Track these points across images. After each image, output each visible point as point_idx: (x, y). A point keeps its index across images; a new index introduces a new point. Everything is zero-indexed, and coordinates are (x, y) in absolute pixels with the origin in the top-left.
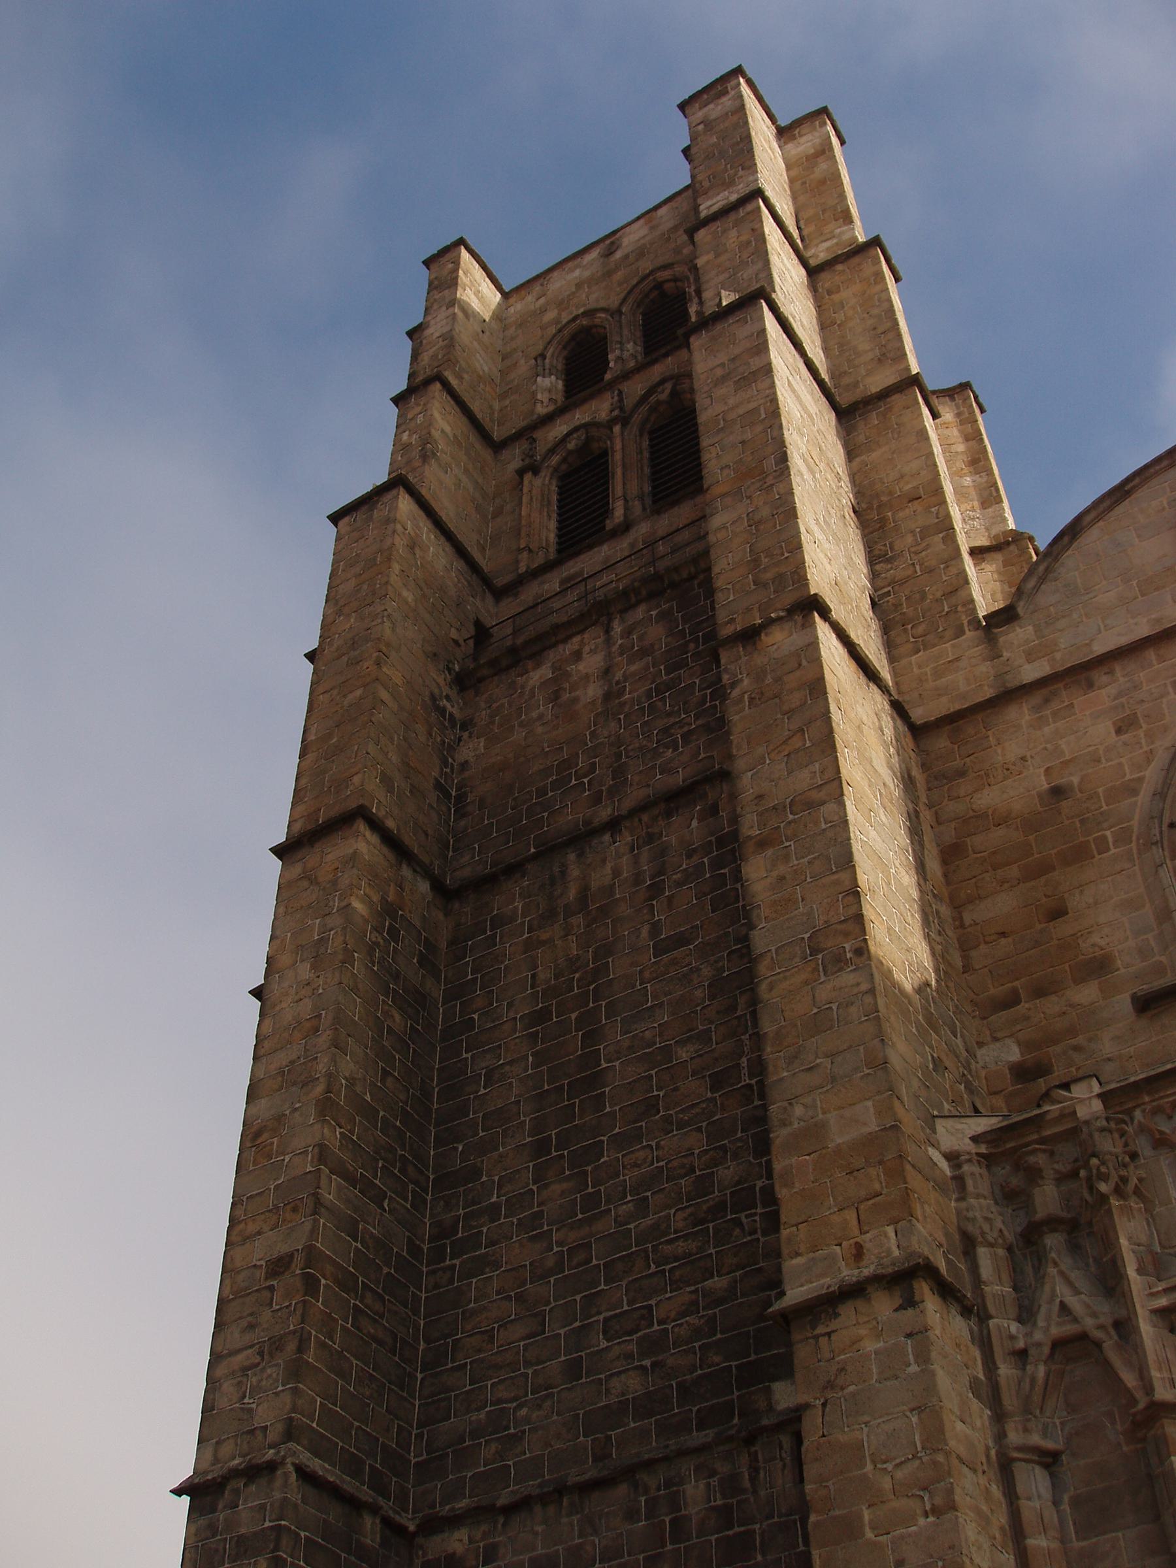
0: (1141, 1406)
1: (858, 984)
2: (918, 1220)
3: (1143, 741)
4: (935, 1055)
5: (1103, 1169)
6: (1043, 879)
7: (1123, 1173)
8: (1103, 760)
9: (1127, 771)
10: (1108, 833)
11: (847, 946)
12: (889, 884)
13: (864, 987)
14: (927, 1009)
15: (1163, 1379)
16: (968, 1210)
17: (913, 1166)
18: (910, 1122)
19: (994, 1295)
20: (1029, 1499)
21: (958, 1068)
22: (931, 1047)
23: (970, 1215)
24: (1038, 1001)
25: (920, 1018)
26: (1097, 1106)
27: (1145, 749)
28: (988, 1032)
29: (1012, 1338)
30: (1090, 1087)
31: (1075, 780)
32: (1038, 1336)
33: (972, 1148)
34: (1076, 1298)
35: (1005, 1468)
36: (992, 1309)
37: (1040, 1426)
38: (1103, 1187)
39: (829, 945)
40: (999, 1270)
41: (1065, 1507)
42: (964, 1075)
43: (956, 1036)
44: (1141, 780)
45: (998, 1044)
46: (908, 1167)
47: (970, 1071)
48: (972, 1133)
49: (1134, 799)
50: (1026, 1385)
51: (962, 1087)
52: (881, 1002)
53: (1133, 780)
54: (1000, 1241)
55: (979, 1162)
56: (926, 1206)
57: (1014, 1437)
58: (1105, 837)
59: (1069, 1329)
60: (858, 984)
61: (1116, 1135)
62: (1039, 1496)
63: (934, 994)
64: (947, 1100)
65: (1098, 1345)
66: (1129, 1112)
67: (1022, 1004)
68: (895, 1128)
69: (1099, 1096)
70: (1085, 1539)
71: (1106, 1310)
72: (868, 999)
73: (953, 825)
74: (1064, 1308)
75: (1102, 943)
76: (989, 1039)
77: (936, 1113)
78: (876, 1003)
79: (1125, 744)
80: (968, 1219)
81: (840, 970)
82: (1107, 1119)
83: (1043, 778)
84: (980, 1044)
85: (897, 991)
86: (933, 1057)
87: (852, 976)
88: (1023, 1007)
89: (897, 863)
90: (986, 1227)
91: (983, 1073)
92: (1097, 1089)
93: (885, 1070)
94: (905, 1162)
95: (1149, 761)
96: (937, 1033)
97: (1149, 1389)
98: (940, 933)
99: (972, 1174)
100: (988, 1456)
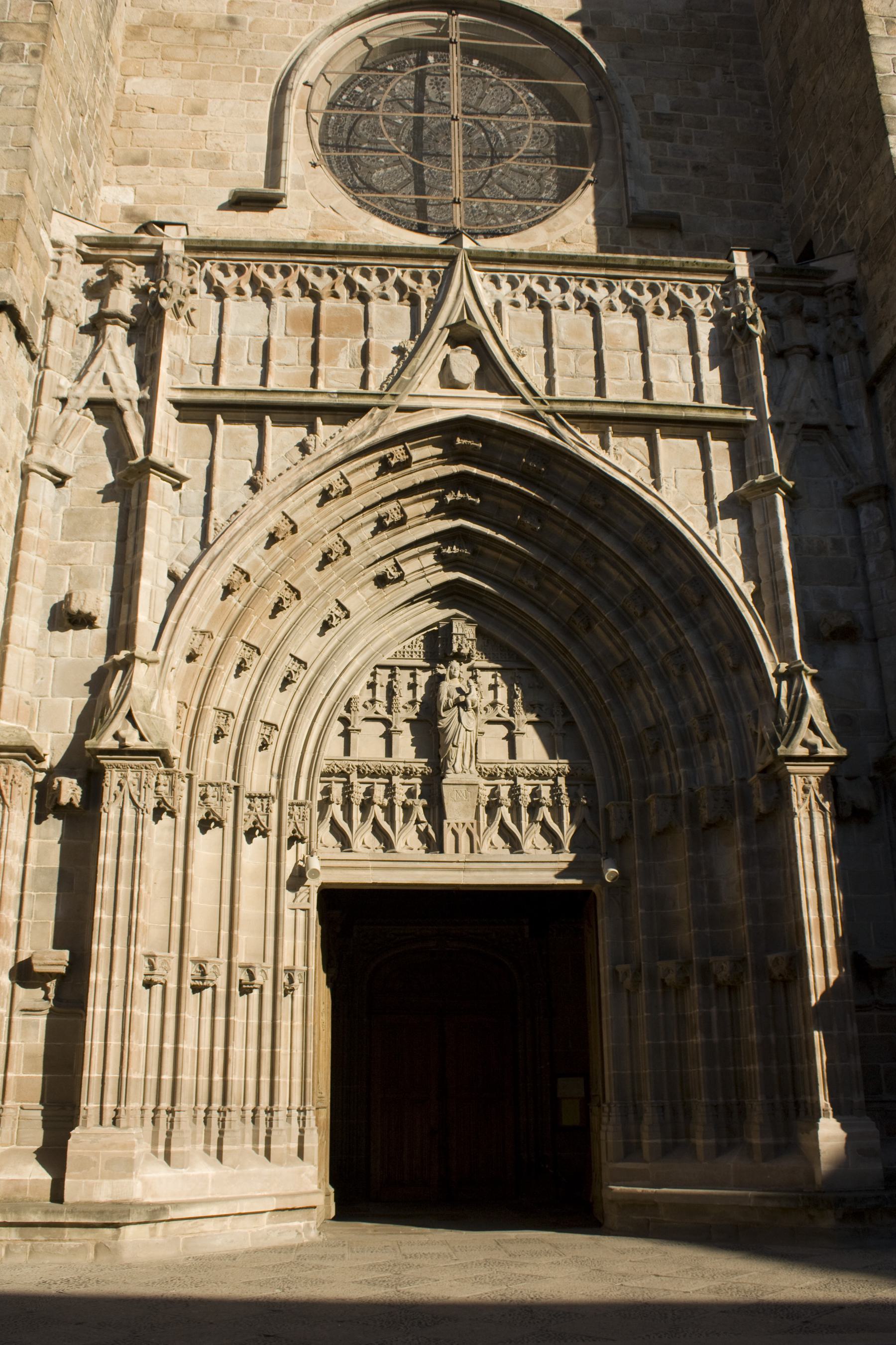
0: (138, 460)
1: (26, 78)
2: (15, 272)
3: (310, 13)
4: (70, 168)
5: (169, 291)
6: (197, 82)
7: (182, 299)
8: (276, 14)
9: (290, 30)
10: (258, 69)
11: (27, 46)
12: (77, 19)
13: (31, 82)
14: (74, 131)
15: (160, 447)
16: (56, 286)
17: (25, 233)
18: (33, 200)
19: (56, 353)
20: (35, 501)
21: (83, 188)
22: (68, 159)
23: (57, 290)
24: (160, 168)
25: (68, 133)
26: (179, 247)
27: (309, 19)
28: (115, 177)
29: (59, 387)
30: (179, 233)
31: (249, 19)
32: (79, 391)
33: (74, 243)
34: (117, 374)
35: (25, 473)
36: (50, 363)
37: (60, 455)
38: (163, 302)
39: (12, 38)
40: (65, 339)
41: (60, 515)
42: (86, 196)
43: (90, 166)
44: (298, 41)
45: (119, 188)
46: (21, 232)
47: (92, 197)
48: (79, 233)
49: (286, 53)
50: (59, 424)
51: (82, 204)
52: (40, 100)
53: (292, 39)
54: (74, 317)
55: (77, 256)
56: (25, 268)
57: (39, 455)
58: (255, 71)
59: (103, 393)
60: (26, 78)
61: (186, 273)
62: (43, 501)
63: (85, 125)
64: (67, 206)
65: (121, 411)
66: (202, 262)
67: (149, 166)
68: (20, 198)
69: (183, 240)
70: (67, 540)
71: (136, 392)
72: (31, 93)
73: (143, 11)
74: (106, 380)
75: (224, 145)
76: (114, 181)
77: (55, 208)
78: (36, 99)
79: (296, 9)
80: (54, 293)
81: (15, 61)
82: (184, 259)
83: (226, 7)
84: (107, 183)
85: (56, 102)
86: (67, 168)
87: (23, 69)
88: (146, 169)
89: (90, 9)
90: (66, 303)
91: (101, 205)
92: (184, 235)
93: (27, 152)
94: (19, 226)
95: (308, 30)
96: (76, 153)
97: (148, 449)
98: (104, 85)
99: (68, 262)
100: (14, 462)
